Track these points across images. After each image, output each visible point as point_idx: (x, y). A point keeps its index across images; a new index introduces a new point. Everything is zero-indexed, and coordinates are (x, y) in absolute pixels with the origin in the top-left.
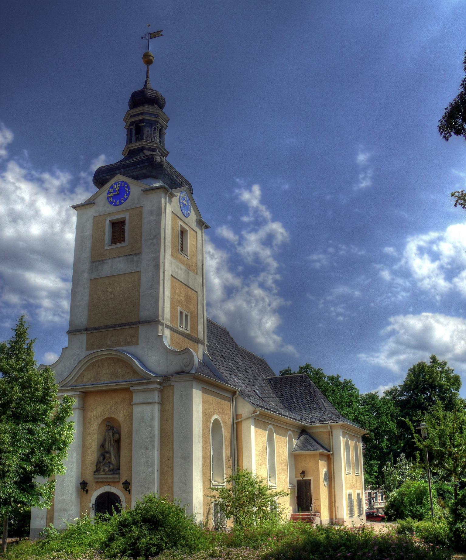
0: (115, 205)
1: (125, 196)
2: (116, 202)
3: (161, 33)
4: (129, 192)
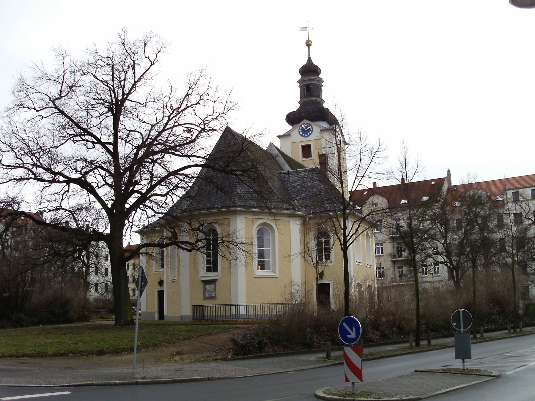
0: (304, 137)
1: (310, 132)
2: (304, 135)
3: (300, 29)
4: (312, 130)
